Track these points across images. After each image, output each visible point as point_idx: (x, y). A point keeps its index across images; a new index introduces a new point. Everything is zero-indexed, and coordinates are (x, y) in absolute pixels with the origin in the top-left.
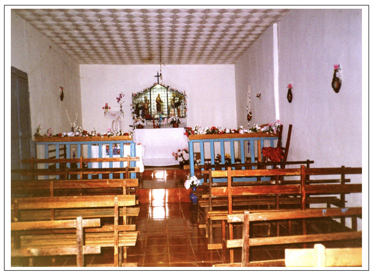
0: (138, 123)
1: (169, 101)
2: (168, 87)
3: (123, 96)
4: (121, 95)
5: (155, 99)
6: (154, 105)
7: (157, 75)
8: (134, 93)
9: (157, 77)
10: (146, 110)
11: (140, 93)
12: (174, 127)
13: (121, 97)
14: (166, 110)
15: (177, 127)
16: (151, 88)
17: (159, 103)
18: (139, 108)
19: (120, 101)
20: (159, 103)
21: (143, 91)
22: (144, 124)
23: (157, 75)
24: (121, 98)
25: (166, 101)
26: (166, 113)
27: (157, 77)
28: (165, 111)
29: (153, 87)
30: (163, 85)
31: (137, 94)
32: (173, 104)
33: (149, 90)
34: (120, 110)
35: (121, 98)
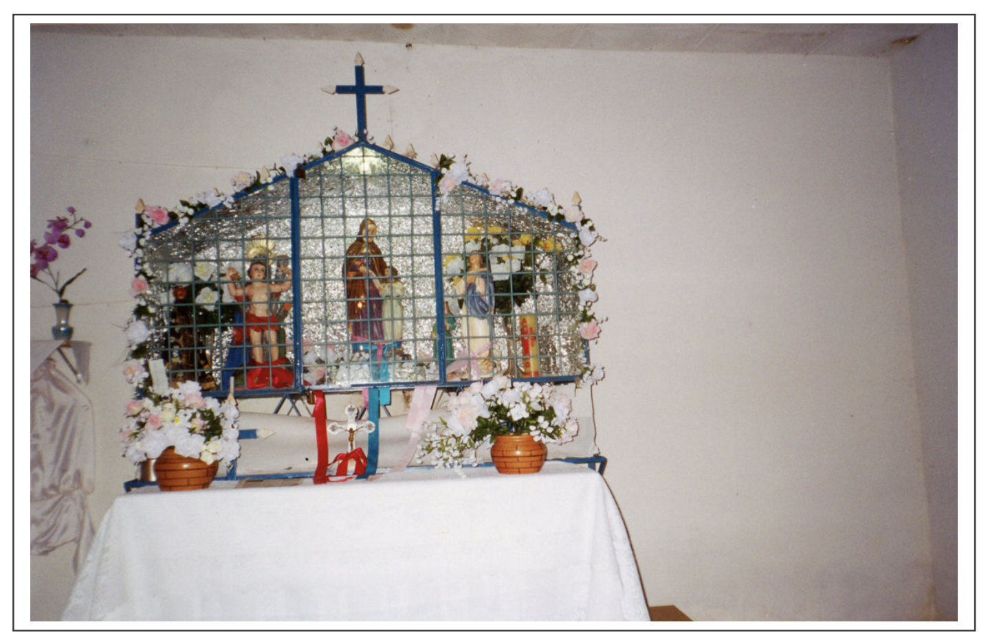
0: (153, 447)
1: (453, 265)
2: (445, 162)
3: (81, 234)
4: (60, 224)
5: (337, 249)
6: (325, 294)
7: (369, 81)
8: (152, 202)
9: (352, 98)
10: (261, 329)
11: (201, 208)
12: (501, 463)
13: (65, 242)
14: (426, 328)
15: (537, 460)
16: (300, 171)
17: (366, 270)
18: (566, 222)
19: (53, 265)
20: (366, 270)
21: (229, 191)
22: (215, 444)
23: (369, 81)
24: (444, 170)
25: (427, 266)
26: (427, 350)
27: (352, 98)
28: (418, 336)
29: (315, 163)
30: (401, 150)
31: (180, 210)
32: (480, 287)
33: (285, 189)
34: (56, 332)
35: (56, 247)
